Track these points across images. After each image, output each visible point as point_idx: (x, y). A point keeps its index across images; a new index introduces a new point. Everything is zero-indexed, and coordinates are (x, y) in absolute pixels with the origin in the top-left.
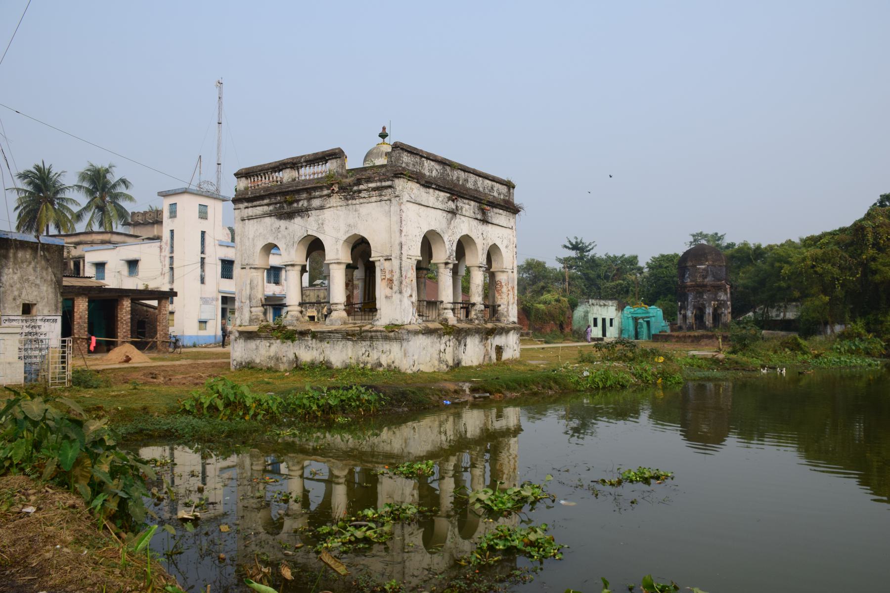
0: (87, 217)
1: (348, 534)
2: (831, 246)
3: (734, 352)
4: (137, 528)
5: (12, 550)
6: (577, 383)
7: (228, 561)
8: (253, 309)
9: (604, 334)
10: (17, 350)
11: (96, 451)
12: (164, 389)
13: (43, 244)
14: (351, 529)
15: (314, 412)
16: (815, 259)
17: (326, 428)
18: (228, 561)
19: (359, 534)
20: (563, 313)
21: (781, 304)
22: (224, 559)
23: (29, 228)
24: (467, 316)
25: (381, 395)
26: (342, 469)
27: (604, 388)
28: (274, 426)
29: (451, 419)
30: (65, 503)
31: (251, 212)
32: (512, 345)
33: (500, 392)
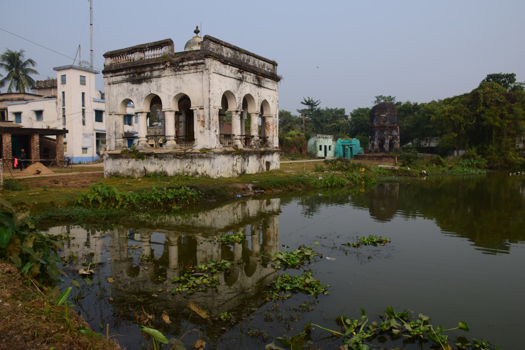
0: (8, 84)
1: (191, 282)
2: (459, 104)
3: (404, 165)
6: (316, 184)
8: (117, 140)
9: (326, 155)
11: (23, 233)
12: (63, 190)
14: (193, 278)
15: (158, 203)
16: (450, 111)
19: (198, 281)
20: (302, 142)
21: (428, 138)
25: (200, 192)
26: (175, 237)
27: (331, 186)
28: (134, 212)
29: (240, 206)
31: (114, 79)
32: (275, 161)
33: (270, 189)
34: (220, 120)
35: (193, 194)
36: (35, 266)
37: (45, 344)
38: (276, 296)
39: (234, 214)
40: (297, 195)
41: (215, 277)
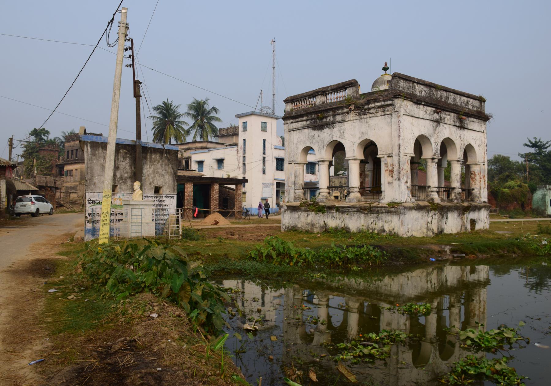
0: (193, 133)
4: (218, 333)
5: (144, 339)
6: (537, 249)
7: (275, 361)
8: (296, 191)
10: (151, 215)
11: (194, 281)
12: (238, 242)
13: (166, 150)
15: (337, 262)
17: (345, 273)
18: (275, 361)
19: (366, 351)
22: (272, 360)
23: (160, 140)
24: (448, 196)
25: (385, 252)
28: (309, 270)
29: (435, 272)
30: (174, 313)
31: (295, 125)
32: (483, 220)
33: (474, 254)
34: (411, 169)
35: (376, 254)
36: (202, 314)
37: (201, 384)
38: (454, 378)
39: (427, 282)
40: (517, 263)
41: (386, 349)
